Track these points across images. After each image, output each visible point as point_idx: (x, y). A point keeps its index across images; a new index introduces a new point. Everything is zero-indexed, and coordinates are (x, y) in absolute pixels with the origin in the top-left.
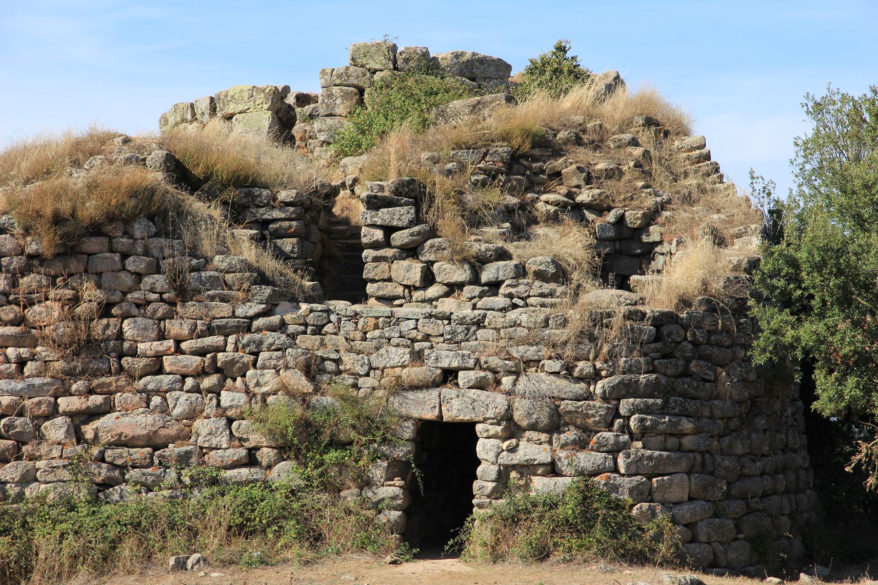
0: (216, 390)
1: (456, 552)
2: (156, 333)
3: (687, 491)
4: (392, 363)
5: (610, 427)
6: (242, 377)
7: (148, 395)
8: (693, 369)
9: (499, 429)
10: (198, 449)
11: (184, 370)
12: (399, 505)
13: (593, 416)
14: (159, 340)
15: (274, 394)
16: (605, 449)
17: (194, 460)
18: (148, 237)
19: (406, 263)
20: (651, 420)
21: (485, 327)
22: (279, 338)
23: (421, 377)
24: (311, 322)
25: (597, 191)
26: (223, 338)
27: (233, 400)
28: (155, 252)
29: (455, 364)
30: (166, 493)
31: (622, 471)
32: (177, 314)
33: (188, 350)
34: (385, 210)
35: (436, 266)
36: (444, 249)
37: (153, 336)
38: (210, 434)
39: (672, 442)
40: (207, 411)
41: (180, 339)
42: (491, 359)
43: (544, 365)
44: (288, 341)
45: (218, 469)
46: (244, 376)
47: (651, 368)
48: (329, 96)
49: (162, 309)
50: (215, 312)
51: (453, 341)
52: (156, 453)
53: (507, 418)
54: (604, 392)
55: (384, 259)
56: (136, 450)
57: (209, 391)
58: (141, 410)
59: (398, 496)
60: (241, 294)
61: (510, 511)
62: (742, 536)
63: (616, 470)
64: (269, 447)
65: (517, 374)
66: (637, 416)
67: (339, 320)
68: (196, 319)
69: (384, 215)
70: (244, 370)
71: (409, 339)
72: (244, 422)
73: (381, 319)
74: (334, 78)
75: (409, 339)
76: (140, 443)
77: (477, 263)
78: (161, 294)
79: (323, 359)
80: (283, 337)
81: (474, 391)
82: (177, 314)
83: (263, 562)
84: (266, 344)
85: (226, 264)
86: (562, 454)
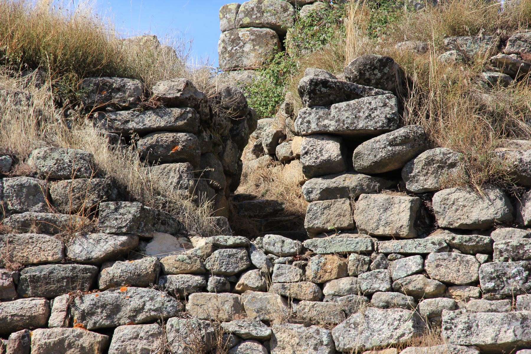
4: (375, 340)
19: (382, 197)
22: (152, 299)
24: (216, 268)
26: (42, 301)
34: (343, 104)
35: (437, 197)
36: (453, 165)
44: (171, 304)
48: (233, 41)
50: (21, 254)
60: (79, 220)
67: (270, 262)
69: (340, 116)
71: (409, 293)
73: (352, 257)
74: (241, 15)
75: (409, 293)
80: (161, 296)
84: (126, 311)
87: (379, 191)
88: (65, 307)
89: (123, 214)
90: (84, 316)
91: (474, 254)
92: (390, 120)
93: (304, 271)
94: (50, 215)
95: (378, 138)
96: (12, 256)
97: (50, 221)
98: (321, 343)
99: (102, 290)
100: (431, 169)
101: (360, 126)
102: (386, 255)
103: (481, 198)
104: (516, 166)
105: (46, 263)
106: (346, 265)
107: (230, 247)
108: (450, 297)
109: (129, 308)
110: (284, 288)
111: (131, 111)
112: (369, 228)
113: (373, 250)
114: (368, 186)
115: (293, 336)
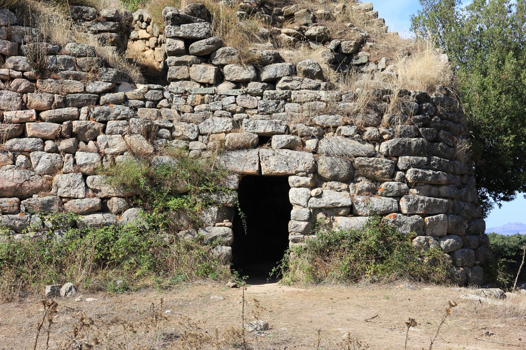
0: (72, 151)
1: (275, 279)
2: (19, 103)
3: (446, 227)
4: (217, 130)
5: (392, 177)
6: (93, 140)
7: (14, 154)
8: (441, 137)
9: (308, 180)
10: (58, 198)
11: (44, 134)
12: (229, 241)
13: (381, 169)
14: (22, 110)
15: (122, 154)
16: (391, 194)
17: (55, 207)
18: (11, 25)
19: (202, 66)
20: (422, 173)
21: (290, 102)
22: (123, 110)
23: (242, 140)
25: (322, 27)
26: (77, 109)
27: (87, 159)
28: (17, 38)
29: (269, 130)
30: (32, 234)
31: (405, 211)
32: (37, 89)
33: (47, 118)
34: (186, 25)
35: (226, 68)
36: (233, 55)
37: (17, 105)
38: (69, 186)
39: (434, 190)
40: (66, 167)
41: (40, 109)
42: (298, 125)
43: (340, 130)
44: (131, 113)
45: (77, 214)
46: (95, 140)
47: (417, 134)
49: (24, 84)
50: (66, 88)
51: (266, 112)
52: (22, 202)
53: (314, 170)
54: (388, 151)
55: (184, 63)
56: (5, 199)
57: (66, 151)
58: (8, 166)
59: (227, 234)
60: (90, 75)
61: (321, 244)
62: (478, 262)
63: (399, 211)
64: (118, 197)
65: (320, 137)
66: (412, 169)
67: (172, 96)
68: (53, 93)
69: (185, 29)
70: (95, 135)
71: (230, 111)
72: (97, 177)
73: (207, 96)
75: (230, 111)
76: (8, 194)
77: (259, 65)
78: (23, 72)
79: (160, 127)
81: (286, 150)
82: (37, 89)
83: (126, 288)
84: (112, 115)
85: (78, 50)
86: (359, 199)
87: (200, 63)
88: (86, 112)
89: (109, 74)
90: (95, 116)
91: (256, 96)
92: (207, 34)
93: (186, 101)
94: (77, 72)
95: (202, 41)
96: (62, 89)
97: (78, 75)
98: (194, 130)
99: (102, 105)
100: (224, 56)
101: (194, 35)
102: (220, 95)
103: (245, 69)
104: (260, 57)
105: (77, 93)
106: (204, 99)
107: (155, 89)
108: (246, 113)
109: (114, 113)
110: (178, 107)
111: (91, 22)
112: (197, 79)
113: (215, 93)
114: (196, 61)
115: (182, 127)
